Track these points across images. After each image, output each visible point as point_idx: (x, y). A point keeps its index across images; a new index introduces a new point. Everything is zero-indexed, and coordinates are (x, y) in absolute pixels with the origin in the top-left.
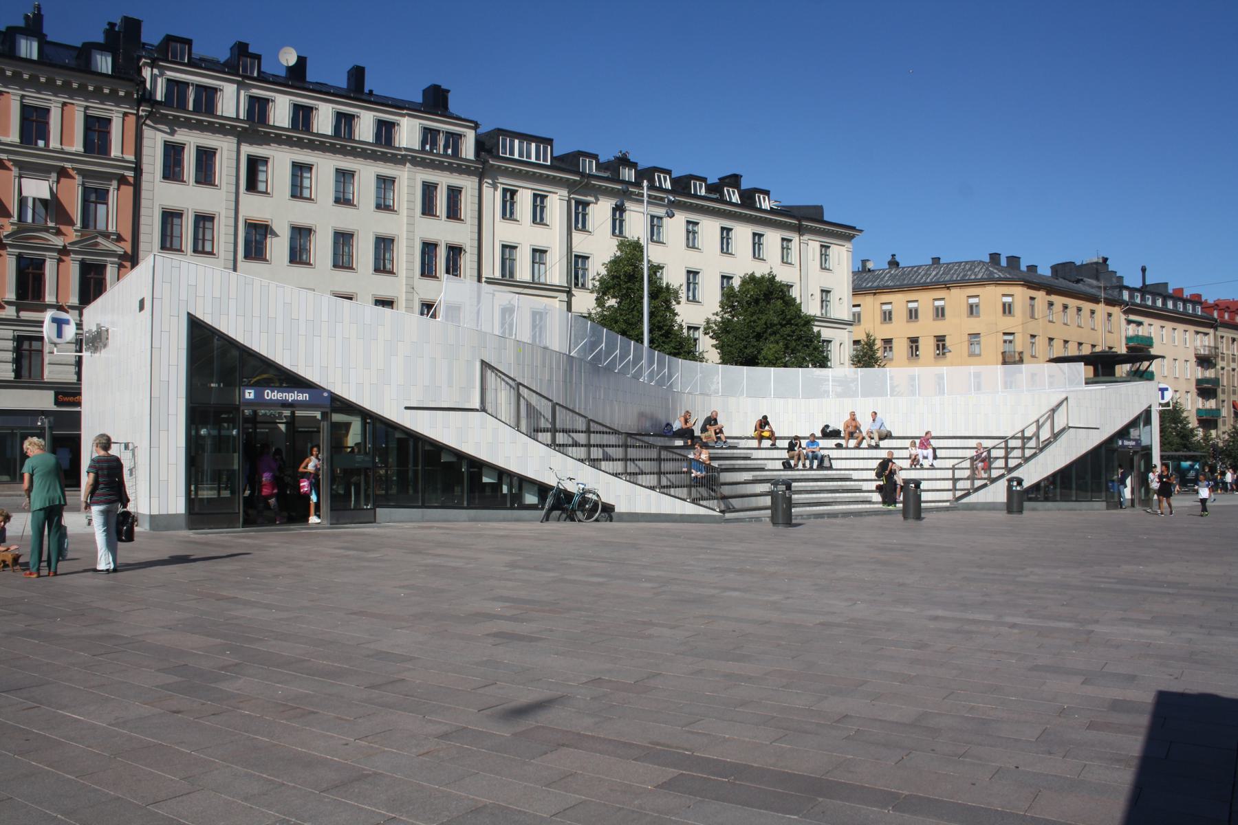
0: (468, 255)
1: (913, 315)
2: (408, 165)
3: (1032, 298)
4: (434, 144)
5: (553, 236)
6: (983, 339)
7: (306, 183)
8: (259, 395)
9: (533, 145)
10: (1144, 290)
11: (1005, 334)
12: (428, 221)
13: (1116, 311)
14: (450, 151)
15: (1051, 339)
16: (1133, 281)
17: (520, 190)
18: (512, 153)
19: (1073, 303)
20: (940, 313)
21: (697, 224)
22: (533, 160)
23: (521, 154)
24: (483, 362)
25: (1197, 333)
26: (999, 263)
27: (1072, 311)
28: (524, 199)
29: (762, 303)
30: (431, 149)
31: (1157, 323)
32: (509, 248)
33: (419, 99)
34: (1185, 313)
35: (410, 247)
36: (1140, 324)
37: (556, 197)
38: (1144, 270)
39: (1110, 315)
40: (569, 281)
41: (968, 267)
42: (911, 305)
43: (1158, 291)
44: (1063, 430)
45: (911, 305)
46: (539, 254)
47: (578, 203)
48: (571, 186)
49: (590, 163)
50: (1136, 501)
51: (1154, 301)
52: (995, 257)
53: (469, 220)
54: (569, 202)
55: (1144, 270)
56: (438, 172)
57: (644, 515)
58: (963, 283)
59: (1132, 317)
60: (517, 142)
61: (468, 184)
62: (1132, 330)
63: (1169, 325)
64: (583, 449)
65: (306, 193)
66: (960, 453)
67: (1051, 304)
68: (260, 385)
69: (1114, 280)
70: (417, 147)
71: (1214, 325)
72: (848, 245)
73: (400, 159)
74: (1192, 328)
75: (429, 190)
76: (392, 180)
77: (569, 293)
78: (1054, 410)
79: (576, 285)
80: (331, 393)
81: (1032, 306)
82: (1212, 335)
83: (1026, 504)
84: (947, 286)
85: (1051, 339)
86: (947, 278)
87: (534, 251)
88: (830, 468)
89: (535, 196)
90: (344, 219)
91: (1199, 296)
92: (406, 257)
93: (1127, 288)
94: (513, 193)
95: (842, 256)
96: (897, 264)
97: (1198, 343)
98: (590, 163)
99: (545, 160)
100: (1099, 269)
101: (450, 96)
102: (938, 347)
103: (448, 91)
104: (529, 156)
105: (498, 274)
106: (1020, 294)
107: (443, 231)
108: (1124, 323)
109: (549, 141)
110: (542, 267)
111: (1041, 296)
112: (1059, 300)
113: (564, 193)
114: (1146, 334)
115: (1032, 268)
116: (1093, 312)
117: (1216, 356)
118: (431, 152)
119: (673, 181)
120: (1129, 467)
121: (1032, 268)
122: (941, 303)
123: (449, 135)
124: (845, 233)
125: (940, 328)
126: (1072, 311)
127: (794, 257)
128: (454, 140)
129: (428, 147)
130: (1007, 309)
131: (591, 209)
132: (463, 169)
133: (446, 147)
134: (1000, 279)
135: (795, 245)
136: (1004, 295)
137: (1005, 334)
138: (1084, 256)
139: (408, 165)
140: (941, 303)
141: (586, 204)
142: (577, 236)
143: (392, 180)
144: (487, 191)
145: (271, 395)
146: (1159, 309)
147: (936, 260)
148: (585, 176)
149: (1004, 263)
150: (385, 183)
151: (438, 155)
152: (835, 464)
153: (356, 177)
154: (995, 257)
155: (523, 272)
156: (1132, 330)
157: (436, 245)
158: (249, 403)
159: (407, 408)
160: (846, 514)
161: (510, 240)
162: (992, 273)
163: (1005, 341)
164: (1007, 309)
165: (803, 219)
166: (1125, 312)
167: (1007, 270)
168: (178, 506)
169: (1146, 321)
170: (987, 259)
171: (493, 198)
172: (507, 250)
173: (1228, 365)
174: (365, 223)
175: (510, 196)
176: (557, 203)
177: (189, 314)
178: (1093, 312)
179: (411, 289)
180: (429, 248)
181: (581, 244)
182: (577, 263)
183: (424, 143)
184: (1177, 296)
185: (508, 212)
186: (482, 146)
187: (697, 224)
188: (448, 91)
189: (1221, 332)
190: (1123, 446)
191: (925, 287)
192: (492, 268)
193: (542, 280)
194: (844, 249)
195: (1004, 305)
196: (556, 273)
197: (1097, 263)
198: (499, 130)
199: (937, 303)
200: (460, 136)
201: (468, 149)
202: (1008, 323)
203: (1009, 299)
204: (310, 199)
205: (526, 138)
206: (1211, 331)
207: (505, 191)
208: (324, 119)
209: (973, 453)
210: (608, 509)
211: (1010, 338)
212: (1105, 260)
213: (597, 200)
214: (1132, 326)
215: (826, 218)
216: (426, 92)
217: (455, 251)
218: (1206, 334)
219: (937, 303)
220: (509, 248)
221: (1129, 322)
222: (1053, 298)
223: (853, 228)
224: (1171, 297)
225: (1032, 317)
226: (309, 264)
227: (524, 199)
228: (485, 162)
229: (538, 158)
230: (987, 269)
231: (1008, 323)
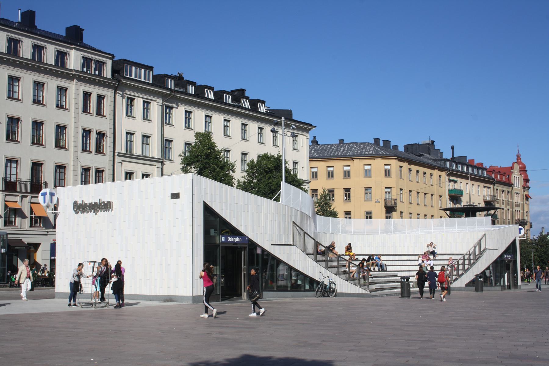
0: (108, 138)
1: (330, 175)
2: (75, 80)
3: (401, 167)
4: (88, 68)
5: (153, 128)
6: (373, 190)
7: (16, 89)
8: (226, 239)
9: (143, 70)
10: (453, 160)
11: (386, 188)
12: (86, 116)
13: (443, 174)
14: (97, 72)
15: (410, 191)
16: (447, 155)
17: (136, 98)
18: (131, 75)
19: (422, 169)
20: (347, 174)
21: (229, 121)
22: (142, 79)
23: (136, 76)
24: (294, 222)
25: (485, 187)
26: (379, 145)
27: (414, 172)
28: (138, 103)
29: (274, 172)
30: (87, 70)
31: (464, 181)
32: (130, 134)
33: (64, 34)
34: (462, 172)
35: (76, 132)
36: (455, 182)
37: (155, 103)
38: (453, 148)
39: (440, 176)
40: (162, 156)
41: (362, 146)
42: (329, 169)
44: (484, 250)
45: (329, 169)
46: (146, 137)
47: (167, 107)
48: (164, 97)
49: (171, 81)
50: (511, 286)
51: (462, 168)
52: (377, 141)
53: (72, 110)
54: (162, 106)
55: (453, 148)
56: (92, 86)
57: (346, 294)
58: (361, 156)
59: (452, 178)
60: (133, 68)
61: (108, 93)
62: (451, 186)
63: (471, 182)
65: (16, 96)
67: (410, 170)
68: (226, 234)
69: (439, 155)
70: (79, 69)
71: (492, 182)
72: (307, 135)
73: (70, 76)
74: (482, 184)
75: (87, 96)
76: (65, 89)
77: (162, 163)
78: (480, 240)
79: (165, 157)
80: (248, 238)
81: (401, 171)
82: (492, 188)
83: (485, 288)
84: (352, 158)
85: (410, 191)
86: (351, 153)
87: (144, 136)
88: (386, 271)
89: (144, 102)
90: (39, 113)
91: (482, 164)
92: (73, 138)
94: (132, 100)
95: (304, 140)
96: (317, 142)
97: (485, 194)
98: (171, 81)
99: (149, 80)
100: (429, 147)
101: (84, 32)
102: (346, 195)
103: (83, 30)
104: (140, 77)
105: (124, 151)
106: (394, 164)
107: (95, 123)
108: (447, 180)
109: (151, 68)
110: (147, 146)
111: (405, 165)
112: (414, 168)
113: (160, 101)
114: (459, 188)
115: (396, 147)
116: (431, 175)
117: (494, 201)
118: (87, 73)
119: (215, 93)
120: (508, 268)
121: (396, 147)
122: (348, 168)
123: (98, 62)
124: (305, 127)
125: (347, 183)
126: (414, 172)
127: (279, 141)
128: (100, 65)
129: (85, 69)
130: (387, 173)
131: (174, 111)
132: (104, 84)
133: (95, 69)
134: (383, 155)
136: (385, 165)
137: (386, 188)
138: (424, 140)
139: (75, 80)
140: (348, 168)
141: (171, 108)
142: (166, 127)
143: (65, 89)
144: (119, 98)
145: (230, 239)
147: (341, 141)
148: (174, 90)
149: (382, 145)
150: (62, 91)
151: (91, 74)
152: (389, 268)
153: (68, 92)
154: (377, 141)
155: (137, 150)
156: (451, 186)
157: (90, 132)
158: (223, 243)
159: (272, 245)
160: (388, 295)
161: (131, 130)
162: (377, 151)
163: (386, 192)
164: (387, 173)
165: (279, 117)
166: (448, 175)
167: (383, 149)
168: (201, 290)
170: (372, 142)
171: (121, 102)
172: (129, 136)
173: (506, 207)
174: (51, 117)
175: (131, 100)
176: (156, 107)
177: (204, 202)
178: (431, 175)
179: (76, 159)
180: (86, 133)
181: (169, 132)
182: (166, 143)
183: (83, 66)
184: (470, 164)
185: (129, 114)
186: (118, 69)
187: (229, 121)
188: (83, 30)
189: (497, 186)
190: (506, 258)
191: (338, 158)
192: (121, 148)
193: (147, 155)
194: (305, 137)
195: (386, 170)
196: (155, 151)
197: (429, 144)
198: (124, 60)
199: (346, 168)
200: (103, 63)
201: (108, 72)
202: (388, 182)
203: (388, 167)
204: (18, 99)
205: (139, 66)
206: (492, 186)
207: (128, 98)
208: (50, 56)
209: (446, 262)
211: (389, 190)
212: (433, 142)
213: (178, 106)
214: (452, 183)
215: (294, 118)
216: (68, 29)
217: (101, 135)
218: (489, 188)
219: (346, 168)
220: (130, 134)
221: (450, 181)
222: (412, 167)
223: (310, 125)
224: (475, 167)
225: (401, 178)
226: (17, 141)
227: (138, 103)
228: (119, 81)
229: (145, 79)
230: (374, 148)
231: (388, 182)
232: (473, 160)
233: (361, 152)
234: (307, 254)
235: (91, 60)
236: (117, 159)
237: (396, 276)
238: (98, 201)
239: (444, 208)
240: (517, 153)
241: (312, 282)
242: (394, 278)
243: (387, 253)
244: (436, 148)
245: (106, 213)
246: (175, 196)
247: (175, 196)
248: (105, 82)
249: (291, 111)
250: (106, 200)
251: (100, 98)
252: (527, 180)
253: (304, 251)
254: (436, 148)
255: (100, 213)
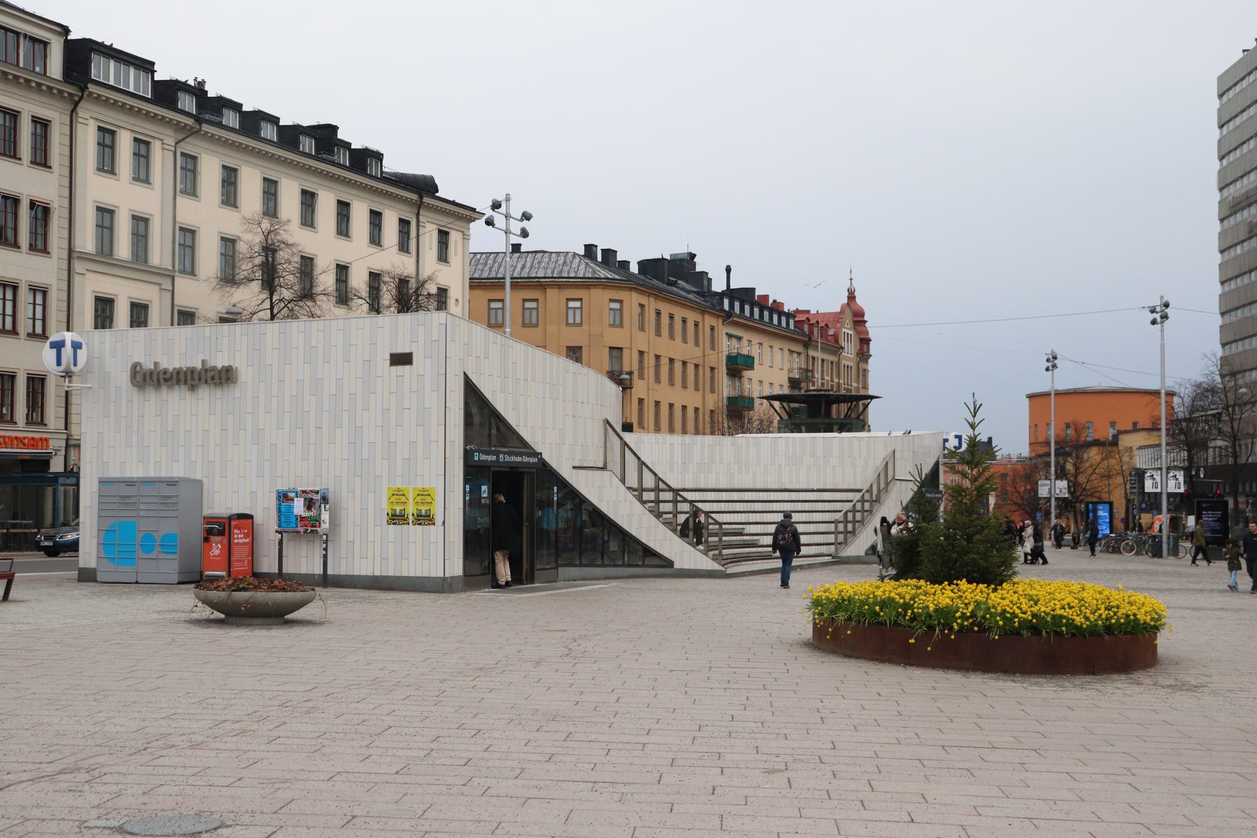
10: (731, 293)
16: (718, 286)
31: (756, 338)
38: (728, 270)
43: (745, 295)
52: (590, 249)
55: (728, 270)
64: (671, 505)
66: (837, 506)
93: (785, 313)
123: (34, 40)
135: (454, 237)
136: (611, 300)
142: (182, 201)
146: (746, 319)
154: (590, 249)
169: (746, 335)
170: (582, 252)
181: (189, 211)
185: (107, 165)
192: (87, 241)
200: (45, 44)
201: (55, 67)
210: (670, 564)
223: (474, 210)
232: (767, 297)
233: (561, 271)
234: (629, 488)
235: (17, 34)
236: (78, 266)
237: (741, 534)
238: (199, 366)
239: (765, 394)
240: (848, 285)
241: (648, 552)
242: (738, 538)
243: (714, 487)
244: (698, 269)
245: (218, 393)
246: (400, 359)
247: (400, 359)
248: (50, 88)
249: (432, 179)
250: (220, 362)
251: (42, 124)
252: (865, 341)
253: (623, 481)
254: (698, 269)
255: (204, 393)
